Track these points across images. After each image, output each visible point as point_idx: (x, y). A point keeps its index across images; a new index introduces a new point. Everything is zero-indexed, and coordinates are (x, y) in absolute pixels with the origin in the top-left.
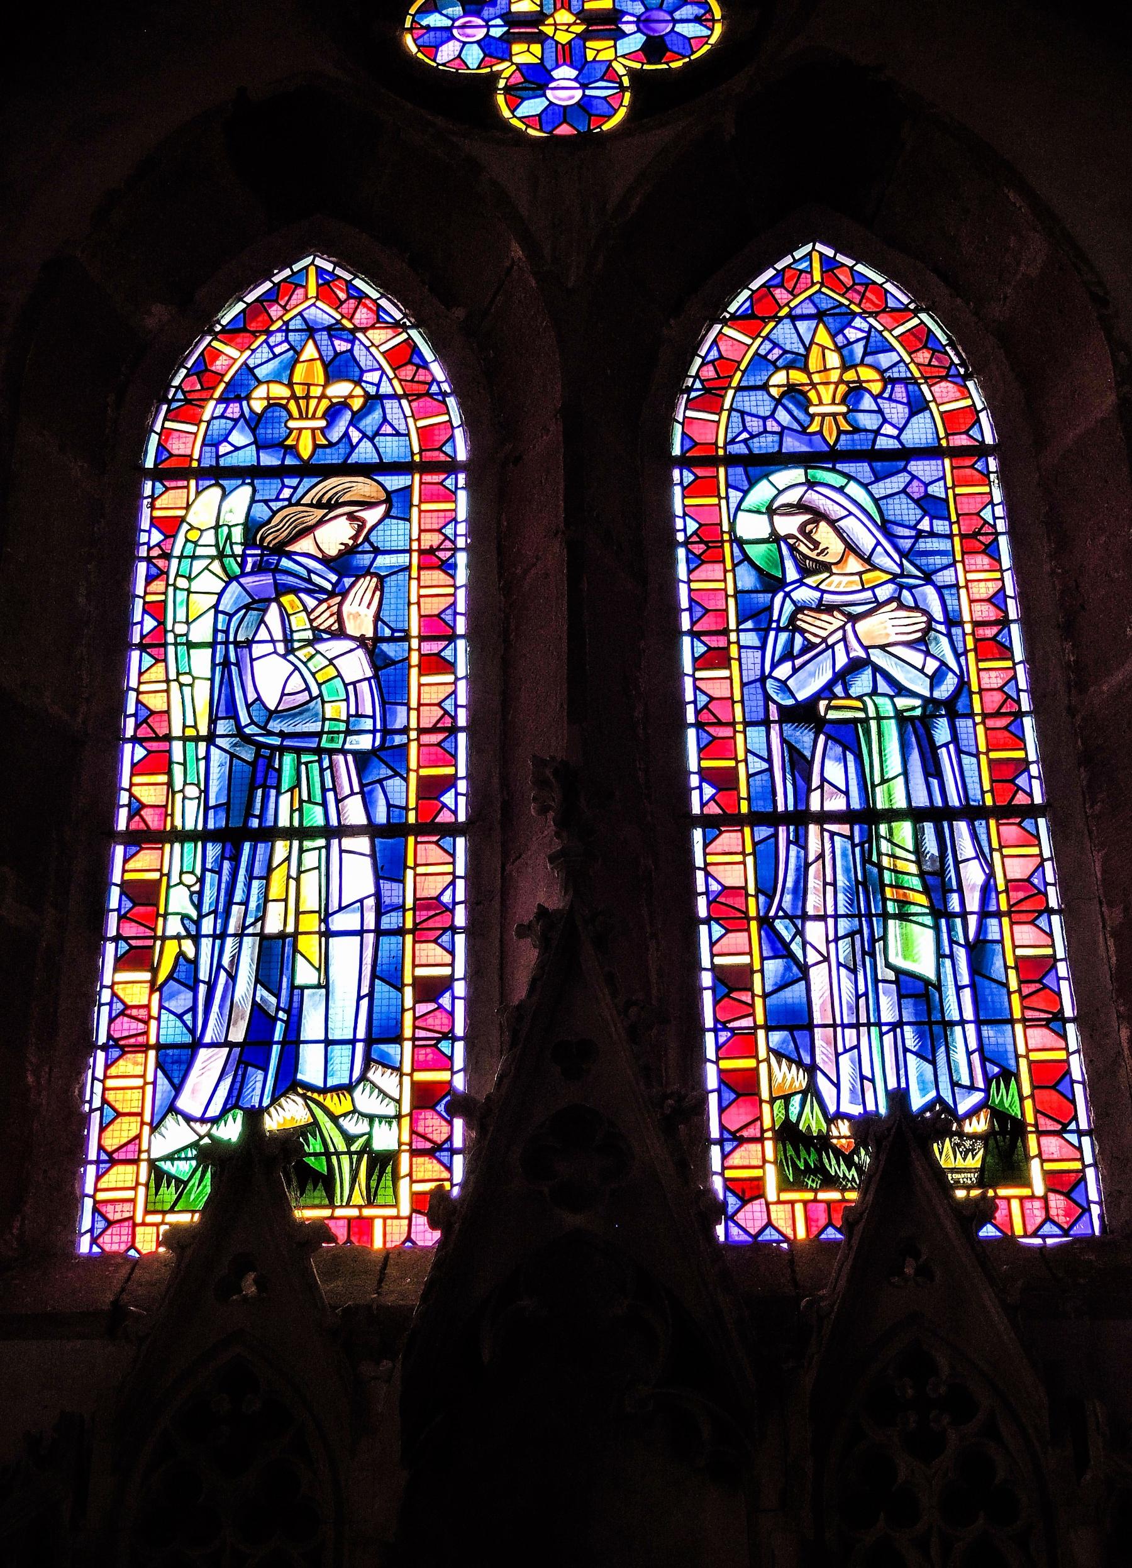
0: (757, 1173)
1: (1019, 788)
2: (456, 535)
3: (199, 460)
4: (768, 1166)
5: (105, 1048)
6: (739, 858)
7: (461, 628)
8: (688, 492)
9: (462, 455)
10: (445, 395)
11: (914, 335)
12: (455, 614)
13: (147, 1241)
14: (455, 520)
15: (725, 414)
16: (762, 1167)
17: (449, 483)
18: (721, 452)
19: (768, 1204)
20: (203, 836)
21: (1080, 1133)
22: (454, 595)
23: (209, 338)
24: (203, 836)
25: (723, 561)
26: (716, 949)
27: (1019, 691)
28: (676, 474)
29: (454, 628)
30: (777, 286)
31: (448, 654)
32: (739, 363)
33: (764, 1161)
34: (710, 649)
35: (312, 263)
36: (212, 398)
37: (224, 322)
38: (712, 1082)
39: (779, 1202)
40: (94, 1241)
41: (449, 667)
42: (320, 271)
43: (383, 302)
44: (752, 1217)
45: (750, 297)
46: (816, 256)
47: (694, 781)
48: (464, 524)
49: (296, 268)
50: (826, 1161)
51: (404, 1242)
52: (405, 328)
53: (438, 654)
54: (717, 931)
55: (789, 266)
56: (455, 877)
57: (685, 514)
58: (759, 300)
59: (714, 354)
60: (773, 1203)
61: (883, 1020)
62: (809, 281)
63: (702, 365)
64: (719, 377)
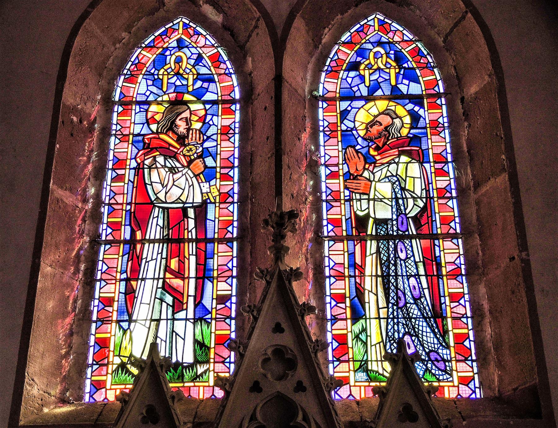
0: (347, 374)
1: (451, 227)
2: (235, 127)
3: (136, 98)
4: (351, 372)
5: (96, 322)
6: (342, 253)
7: (449, 159)
8: (119, 114)
9: (237, 97)
10: (231, 73)
11: (419, 50)
12: (234, 158)
13: (111, 396)
14: (234, 122)
15: (340, 80)
16: (349, 372)
17: (438, 102)
18: (134, 99)
19: (350, 386)
20: (159, 241)
21: (472, 361)
22: (234, 151)
23: (140, 50)
24: (159, 241)
25: (337, 138)
26: (332, 287)
27: (451, 189)
28: (320, 103)
29: (234, 164)
30: (360, 31)
31: (231, 174)
32: (345, 61)
33: (350, 370)
34: (332, 172)
35: (375, 17)
36: (342, 69)
37: (146, 43)
38: (92, 343)
39: (355, 386)
40: (91, 396)
41: (447, 174)
42: (184, 24)
43: (405, 32)
44: (344, 392)
45: (350, 35)
46: (376, 20)
47: (325, 223)
48: (238, 123)
49: (175, 22)
50: (185, 373)
51: (457, 396)
52: (217, 47)
53: (227, 174)
54: (333, 280)
55: (365, 23)
56: (460, 255)
57: (117, 123)
58: (354, 36)
59: (336, 57)
60: (109, 390)
61: (381, 316)
62: (373, 30)
63: (331, 61)
64: (338, 66)
